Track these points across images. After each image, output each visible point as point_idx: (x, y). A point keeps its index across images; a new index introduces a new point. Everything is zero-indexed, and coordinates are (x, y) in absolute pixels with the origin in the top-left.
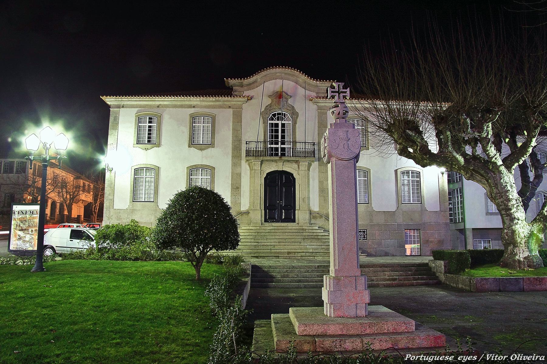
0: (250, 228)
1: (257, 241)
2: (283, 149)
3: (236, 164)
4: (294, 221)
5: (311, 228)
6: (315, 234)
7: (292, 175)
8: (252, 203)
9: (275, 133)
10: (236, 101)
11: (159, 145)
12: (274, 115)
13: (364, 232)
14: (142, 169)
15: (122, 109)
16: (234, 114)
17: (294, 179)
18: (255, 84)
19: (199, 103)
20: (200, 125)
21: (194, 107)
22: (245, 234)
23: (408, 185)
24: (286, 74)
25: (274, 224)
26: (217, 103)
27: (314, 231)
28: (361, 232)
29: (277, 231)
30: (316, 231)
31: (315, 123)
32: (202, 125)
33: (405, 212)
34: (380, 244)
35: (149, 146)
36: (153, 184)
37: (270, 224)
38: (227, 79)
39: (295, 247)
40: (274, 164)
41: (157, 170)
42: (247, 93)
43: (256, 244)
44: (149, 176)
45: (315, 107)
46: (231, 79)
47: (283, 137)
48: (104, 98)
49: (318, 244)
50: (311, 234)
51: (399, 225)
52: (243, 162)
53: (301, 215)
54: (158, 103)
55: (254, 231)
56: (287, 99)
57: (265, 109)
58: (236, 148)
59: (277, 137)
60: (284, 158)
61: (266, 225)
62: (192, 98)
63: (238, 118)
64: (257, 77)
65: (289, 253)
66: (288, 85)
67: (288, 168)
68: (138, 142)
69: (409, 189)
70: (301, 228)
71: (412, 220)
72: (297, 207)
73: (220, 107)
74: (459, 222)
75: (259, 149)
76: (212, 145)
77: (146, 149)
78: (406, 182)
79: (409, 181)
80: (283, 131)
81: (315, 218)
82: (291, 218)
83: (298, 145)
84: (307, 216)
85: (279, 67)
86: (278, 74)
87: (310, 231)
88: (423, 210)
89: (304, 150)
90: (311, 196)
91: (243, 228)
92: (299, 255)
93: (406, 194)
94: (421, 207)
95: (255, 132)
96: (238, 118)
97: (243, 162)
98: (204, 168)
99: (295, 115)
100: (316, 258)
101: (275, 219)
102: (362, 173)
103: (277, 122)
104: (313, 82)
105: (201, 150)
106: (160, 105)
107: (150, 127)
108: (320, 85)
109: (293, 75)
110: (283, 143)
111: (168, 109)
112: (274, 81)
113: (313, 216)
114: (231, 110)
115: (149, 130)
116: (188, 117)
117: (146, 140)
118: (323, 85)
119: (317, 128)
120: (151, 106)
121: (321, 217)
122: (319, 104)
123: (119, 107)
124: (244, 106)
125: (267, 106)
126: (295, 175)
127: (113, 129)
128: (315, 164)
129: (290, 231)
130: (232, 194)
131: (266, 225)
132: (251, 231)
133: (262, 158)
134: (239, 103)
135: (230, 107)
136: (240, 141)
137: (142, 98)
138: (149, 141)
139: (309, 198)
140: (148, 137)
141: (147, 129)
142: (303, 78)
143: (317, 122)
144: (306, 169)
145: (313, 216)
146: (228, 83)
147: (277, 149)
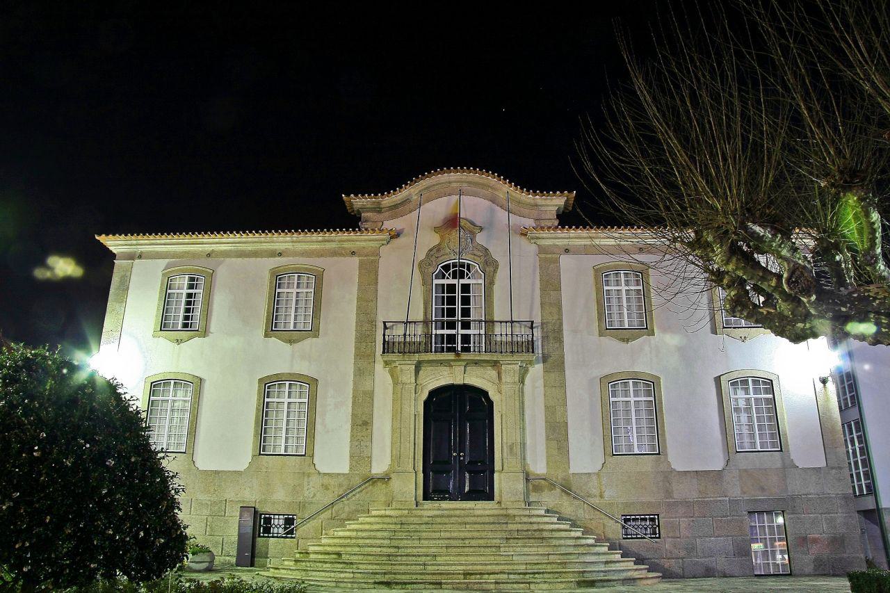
0: (388, 513)
1: (395, 543)
2: (466, 339)
3: (363, 371)
4: (490, 496)
5: (527, 513)
6: (535, 527)
7: (485, 394)
8: (397, 458)
9: (453, 305)
10: (365, 241)
11: (205, 333)
12: (446, 268)
13: (652, 520)
14: (166, 382)
15: (137, 261)
16: (362, 265)
17: (491, 403)
18: (407, 207)
19: (289, 246)
20: (290, 291)
21: (280, 254)
22: (375, 527)
23: (748, 410)
24: (469, 183)
25: (446, 504)
26: (329, 246)
27: (534, 520)
28: (645, 520)
29: (446, 520)
30: (539, 520)
31: (533, 284)
32: (294, 290)
33: (746, 470)
34: (691, 549)
35: (184, 335)
36: (187, 415)
37: (436, 504)
38: (348, 195)
39: (483, 558)
40: (445, 371)
41: (197, 384)
42: (389, 225)
43: (392, 550)
44: (182, 398)
45: (533, 248)
46: (356, 195)
47: (466, 312)
48: (102, 239)
49: (541, 551)
50: (525, 527)
51: (734, 502)
52: (379, 366)
53: (505, 482)
54: (208, 248)
55: (394, 520)
56: (473, 234)
57: (427, 255)
58: (364, 338)
59: (452, 313)
60: (465, 356)
61: (425, 507)
62: (276, 235)
63: (370, 271)
64: (409, 192)
65: (466, 574)
66: (473, 208)
67: (476, 378)
68: (164, 326)
69: (750, 418)
70: (504, 512)
71: (763, 489)
72: (497, 466)
73: (334, 253)
74: (862, 495)
75: (504, 339)
76: (314, 332)
77: (178, 342)
78: (742, 404)
79: (748, 400)
80: (466, 301)
81: (538, 489)
82: (483, 491)
83: (497, 329)
84: (521, 486)
85: (442, 172)
86: (454, 185)
87: (525, 520)
88: (788, 466)
89: (509, 339)
90: (528, 442)
91: (374, 513)
92: (492, 578)
93: (745, 431)
94: (783, 460)
95: (406, 301)
96: (370, 271)
97: (379, 366)
98: (295, 379)
99: (490, 265)
100: (532, 586)
101: (448, 492)
102: (641, 387)
103: (452, 281)
104: (527, 197)
105: (290, 342)
106: (213, 251)
107: (189, 296)
108: (543, 203)
109: (484, 186)
110: (466, 325)
111: (228, 260)
112: (445, 198)
113: (534, 486)
114: (356, 260)
115: (188, 303)
116: (267, 276)
117: (181, 321)
118: (548, 202)
119: (538, 292)
120: (194, 255)
121: (552, 486)
122: (539, 242)
123: (131, 257)
124: (384, 251)
125: (431, 250)
126: (493, 395)
127: (117, 301)
128: (537, 370)
129: (479, 520)
130: (352, 436)
131: (425, 507)
132: (388, 520)
133: (417, 357)
134: (371, 244)
135: (353, 253)
136: (373, 323)
137: (176, 238)
138: (185, 325)
139: (523, 445)
140: (184, 317)
141: (184, 299)
142: (505, 189)
143: (538, 278)
144: (517, 379)
145: (534, 486)
146: (351, 204)
147: (451, 339)
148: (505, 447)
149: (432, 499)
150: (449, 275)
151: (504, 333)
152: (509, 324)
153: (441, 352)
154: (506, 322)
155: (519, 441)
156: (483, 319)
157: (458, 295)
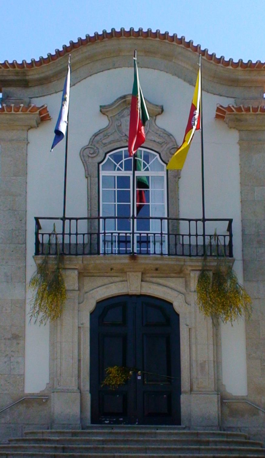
2: (144, 242)
103: (124, 173)
125: (96, 135)
148: (194, 365)
149: (101, 422)
150: (121, 165)
151: (193, 232)
152: (200, 223)
153: (91, 253)
154: (197, 220)
155: (212, 359)
156: (166, 216)
157: (132, 190)
